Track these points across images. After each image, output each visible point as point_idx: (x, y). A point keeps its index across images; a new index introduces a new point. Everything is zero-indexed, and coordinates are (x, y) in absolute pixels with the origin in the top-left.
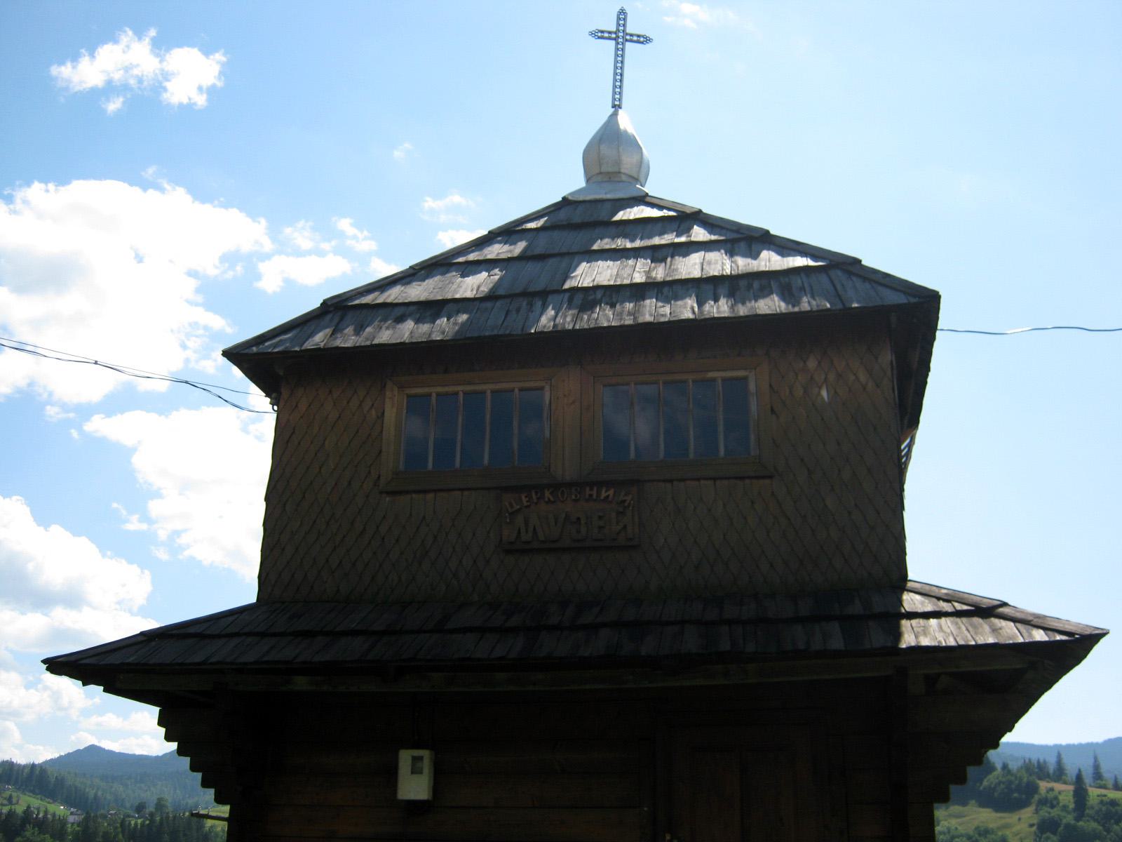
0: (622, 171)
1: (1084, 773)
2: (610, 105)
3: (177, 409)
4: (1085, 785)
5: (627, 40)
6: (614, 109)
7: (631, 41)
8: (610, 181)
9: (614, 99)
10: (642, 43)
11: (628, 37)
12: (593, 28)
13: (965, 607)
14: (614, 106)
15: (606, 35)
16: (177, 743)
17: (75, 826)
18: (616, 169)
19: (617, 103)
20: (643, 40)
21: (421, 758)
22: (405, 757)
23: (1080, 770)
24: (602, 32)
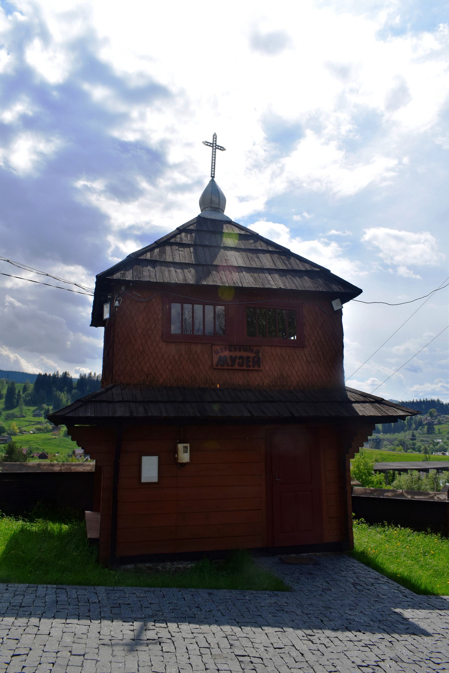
0: (220, 208)
1: (86, 374)
2: (210, 176)
3: (406, 402)
4: (31, 365)
5: (217, 148)
6: (211, 178)
7: (211, 143)
8: (215, 211)
9: (212, 174)
10: (222, 150)
11: (217, 147)
12: (204, 140)
13: (372, 400)
14: (212, 177)
15: (209, 144)
16: (76, 441)
17: (393, 527)
18: (217, 206)
19: (213, 175)
20: (222, 149)
21: (187, 447)
22: (181, 446)
23: (85, 374)
24: (208, 143)
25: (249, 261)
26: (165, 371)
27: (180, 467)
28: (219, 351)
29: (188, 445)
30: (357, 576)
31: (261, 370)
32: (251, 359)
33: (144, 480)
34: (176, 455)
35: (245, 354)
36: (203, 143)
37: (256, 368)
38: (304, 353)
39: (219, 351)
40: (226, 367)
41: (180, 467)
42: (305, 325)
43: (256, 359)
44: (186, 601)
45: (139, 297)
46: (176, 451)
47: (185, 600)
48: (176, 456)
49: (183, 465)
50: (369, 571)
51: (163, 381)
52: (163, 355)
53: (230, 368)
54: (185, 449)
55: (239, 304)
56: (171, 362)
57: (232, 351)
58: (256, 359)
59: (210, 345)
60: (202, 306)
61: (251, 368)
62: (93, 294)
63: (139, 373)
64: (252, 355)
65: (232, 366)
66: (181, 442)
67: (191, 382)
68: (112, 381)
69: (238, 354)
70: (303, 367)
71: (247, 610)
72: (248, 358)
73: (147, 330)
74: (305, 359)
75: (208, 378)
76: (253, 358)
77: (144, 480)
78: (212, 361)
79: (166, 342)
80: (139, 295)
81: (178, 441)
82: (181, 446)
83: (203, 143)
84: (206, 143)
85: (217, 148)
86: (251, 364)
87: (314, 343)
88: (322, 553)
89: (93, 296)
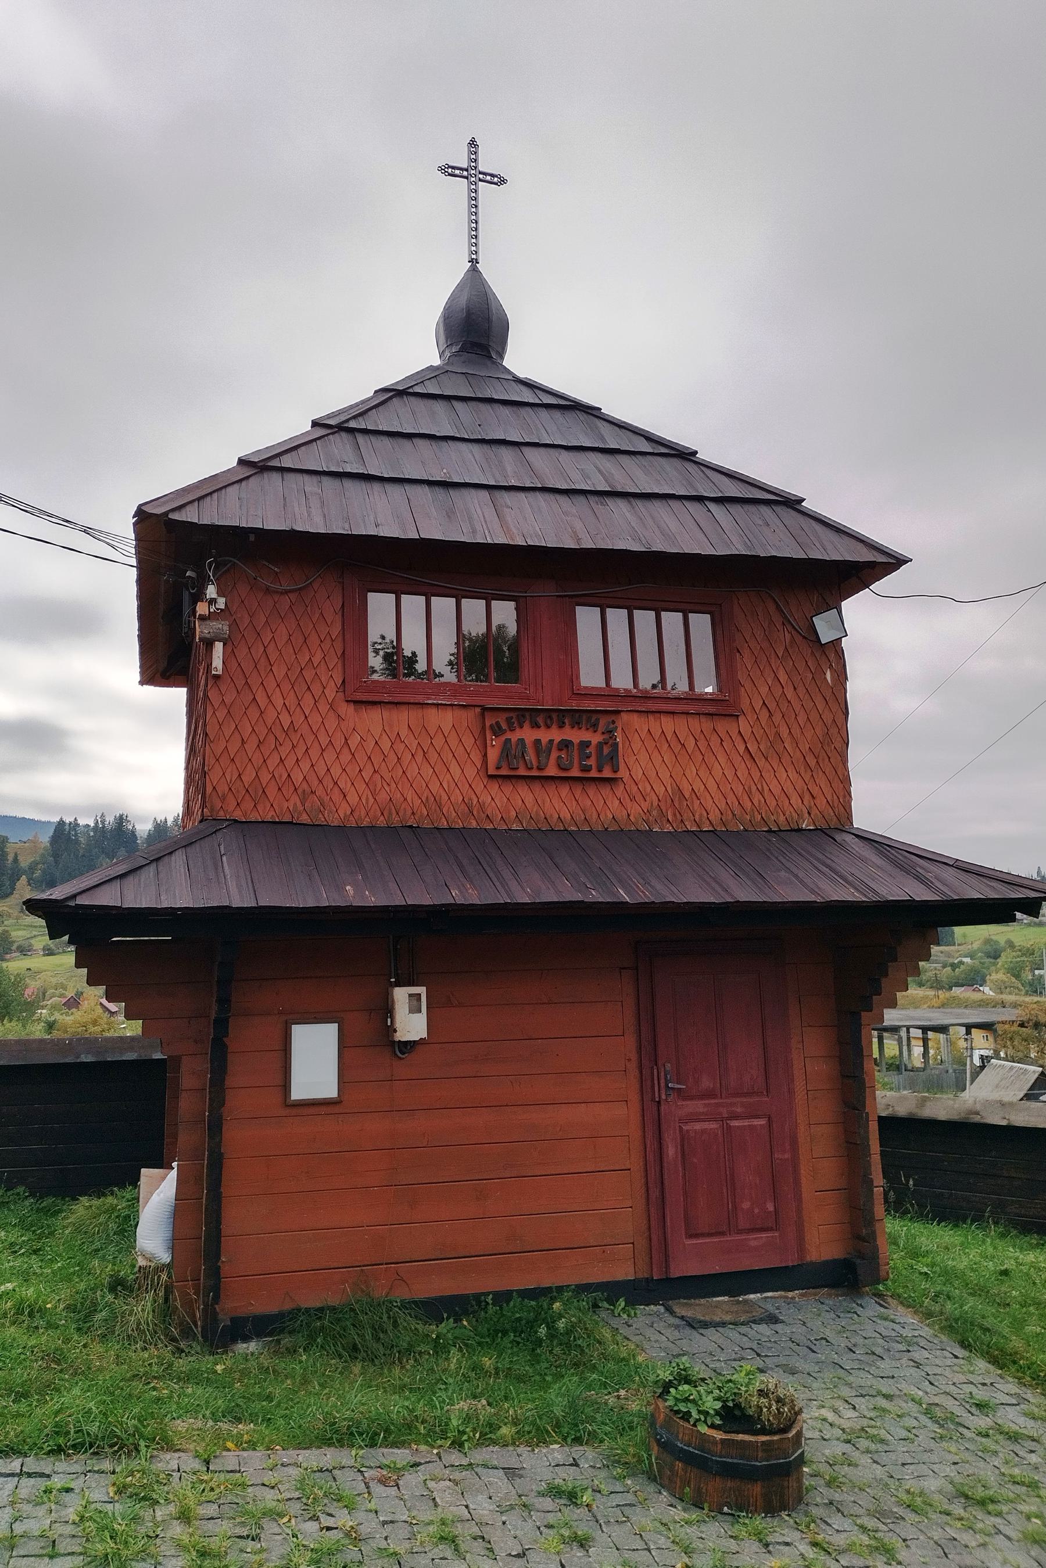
5: (480, 180)
22: (401, 995)
24: (453, 168)
25: (184, 844)
26: (353, 784)
27: (400, 1055)
28: (504, 726)
29: (422, 990)
30: (928, 1375)
31: (622, 778)
32: (591, 750)
33: (298, 1092)
34: (389, 1020)
35: (576, 736)
36: (441, 169)
37: (607, 773)
38: (739, 731)
39: (504, 726)
40: (522, 772)
41: (400, 1055)
42: (739, 652)
43: (606, 750)
44: (440, 1509)
45: (277, 573)
46: (388, 1010)
47: (436, 1505)
48: (389, 1024)
49: (408, 1046)
50: (956, 1357)
51: (349, 812)
52: (346, 739)
53: (535, 773)
54: (415, 1003)
55: (557, 596)
56: (369, 758)
57: (539, 727)
58: (606, 750)
59: (478, 710)
60: (452, 601)
61: (594, 774)
62: (134, 562)
63: (279, 789)
64: (595, 739)
65: (539, 769)
66: (398, 984)
67: (426, 813)
68: (203, 811)
69: (556, 735)
70: (736, 770)
71: (639, 1544)
72: (586, 744)
73: (302, 669)
74: (741, 748)
75: (475, 801)
76: (600, 746)
77: (298, 1092)
78: (485, 755)
79: (355, 702)
80: (276, 569)
81: (392, 980)
82: (401, 995)
83: (441, 169)
84: (450, 170)
85: (480, 180)
86: (592, 762)
87: (764, 701)
88: (801, 1291)
89: (135, 569)
